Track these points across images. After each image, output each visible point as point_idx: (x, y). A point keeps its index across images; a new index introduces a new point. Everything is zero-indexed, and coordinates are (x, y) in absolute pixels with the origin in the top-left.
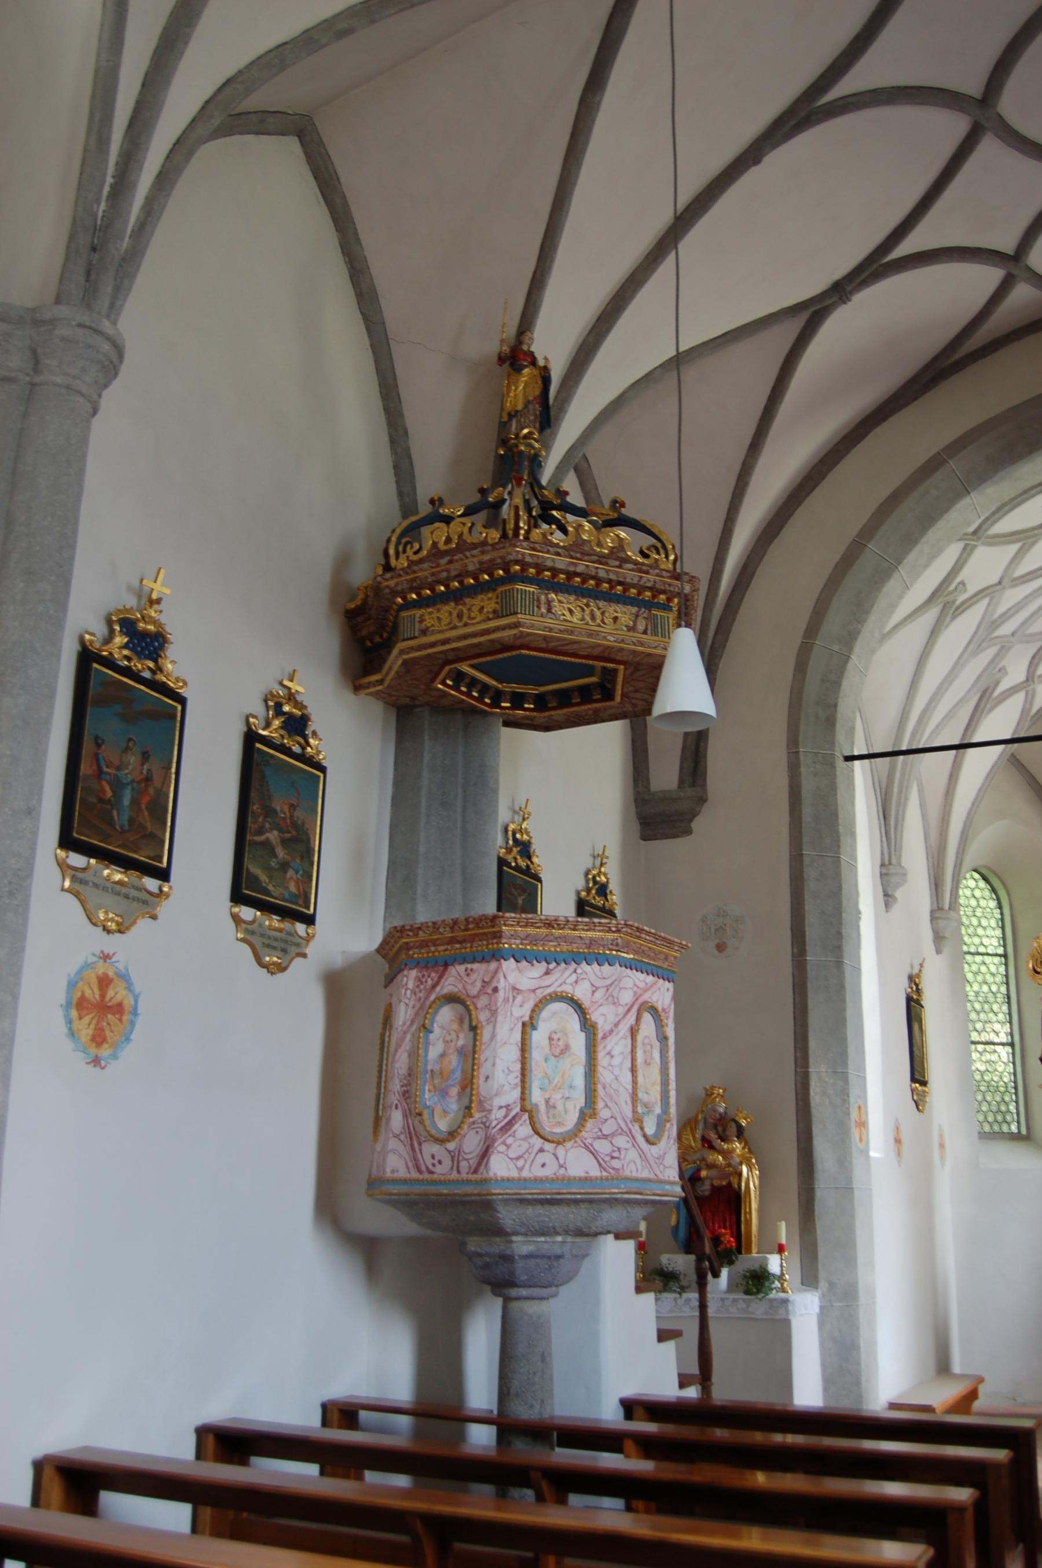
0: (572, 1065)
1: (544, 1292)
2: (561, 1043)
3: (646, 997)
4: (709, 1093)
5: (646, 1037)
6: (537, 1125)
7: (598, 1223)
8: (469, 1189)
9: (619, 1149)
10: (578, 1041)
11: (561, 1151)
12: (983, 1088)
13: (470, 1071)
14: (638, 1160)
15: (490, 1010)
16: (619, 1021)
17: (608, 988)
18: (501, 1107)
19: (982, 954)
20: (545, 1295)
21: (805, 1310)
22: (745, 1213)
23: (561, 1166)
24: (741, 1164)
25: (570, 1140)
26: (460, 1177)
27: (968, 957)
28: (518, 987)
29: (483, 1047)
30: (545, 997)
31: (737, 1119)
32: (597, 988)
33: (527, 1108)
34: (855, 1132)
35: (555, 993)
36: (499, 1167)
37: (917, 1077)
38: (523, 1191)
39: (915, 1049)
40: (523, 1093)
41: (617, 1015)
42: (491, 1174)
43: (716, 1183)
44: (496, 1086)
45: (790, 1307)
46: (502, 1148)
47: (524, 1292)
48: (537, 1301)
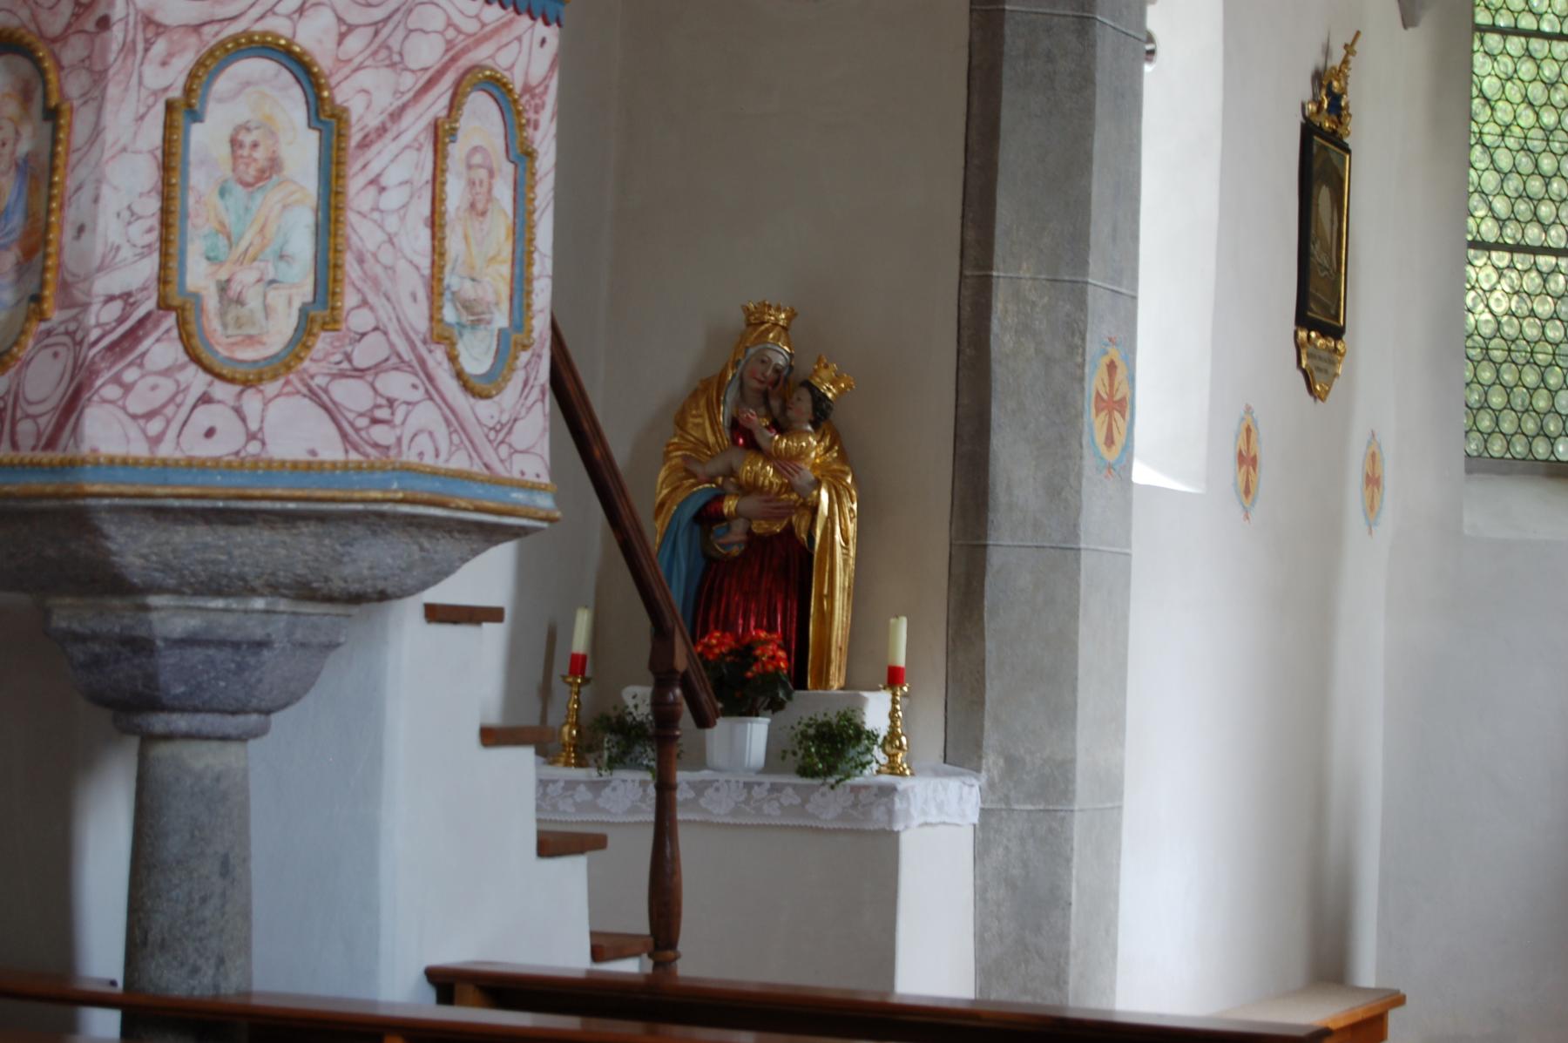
0: (285, 207)
1: (230, 724)
2: (260, 154)
3: (480, 55)
4: (755, 321)
5: (476, 149)
6: (196, 342)
7: (348, 570)
8: (36, 483)
9: (391, 402)
10: (301, 150)
11: (252, 403)
12: (1498, 355)
13: (43, 213)
14: (441, 431)
15: (90, 70)
16: (403, 108)
17: (377, 26)
18: (111, 299)
19: (1528, 34)
20: (231, 731)
21: (938, 827)
22: (820, 598)
23: (251, 437)
24: (817, 484)
25: (275, 377)
26: (16, 457)
27: (1493, 40)
28: (159, 17)
29: (74, 157)
30: (222, 44)
31: (816, 381)
32: (351, 28)
33: (174, 304)
34: (1095, 424)
35: (248, 35)
36: (106, 432)
37: (1315, 313)
38: (159, 491)
39: (1315, 249)
40: (163, 266)
41: (397, 93)
42: (85, 449)
43: (759, 527)
44: (100, 249)
45: (898, 805)
46: (112, 392)
47: (181, 722)
48: (215, 745)
